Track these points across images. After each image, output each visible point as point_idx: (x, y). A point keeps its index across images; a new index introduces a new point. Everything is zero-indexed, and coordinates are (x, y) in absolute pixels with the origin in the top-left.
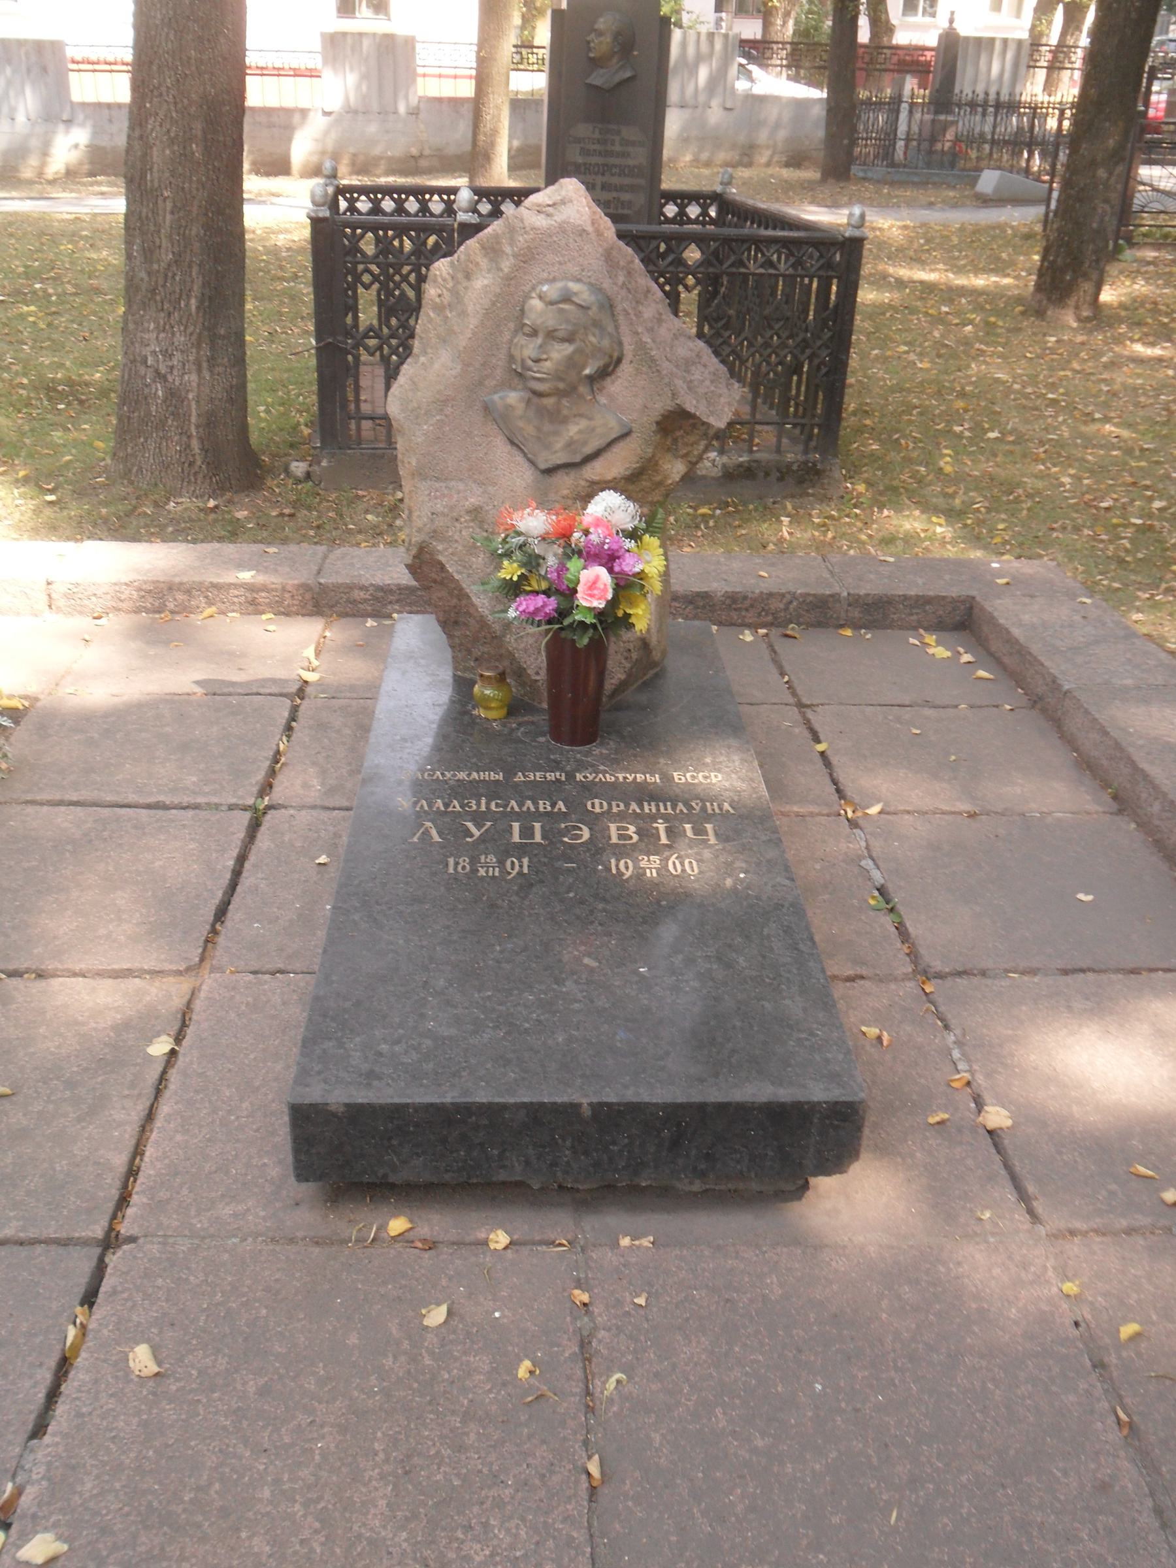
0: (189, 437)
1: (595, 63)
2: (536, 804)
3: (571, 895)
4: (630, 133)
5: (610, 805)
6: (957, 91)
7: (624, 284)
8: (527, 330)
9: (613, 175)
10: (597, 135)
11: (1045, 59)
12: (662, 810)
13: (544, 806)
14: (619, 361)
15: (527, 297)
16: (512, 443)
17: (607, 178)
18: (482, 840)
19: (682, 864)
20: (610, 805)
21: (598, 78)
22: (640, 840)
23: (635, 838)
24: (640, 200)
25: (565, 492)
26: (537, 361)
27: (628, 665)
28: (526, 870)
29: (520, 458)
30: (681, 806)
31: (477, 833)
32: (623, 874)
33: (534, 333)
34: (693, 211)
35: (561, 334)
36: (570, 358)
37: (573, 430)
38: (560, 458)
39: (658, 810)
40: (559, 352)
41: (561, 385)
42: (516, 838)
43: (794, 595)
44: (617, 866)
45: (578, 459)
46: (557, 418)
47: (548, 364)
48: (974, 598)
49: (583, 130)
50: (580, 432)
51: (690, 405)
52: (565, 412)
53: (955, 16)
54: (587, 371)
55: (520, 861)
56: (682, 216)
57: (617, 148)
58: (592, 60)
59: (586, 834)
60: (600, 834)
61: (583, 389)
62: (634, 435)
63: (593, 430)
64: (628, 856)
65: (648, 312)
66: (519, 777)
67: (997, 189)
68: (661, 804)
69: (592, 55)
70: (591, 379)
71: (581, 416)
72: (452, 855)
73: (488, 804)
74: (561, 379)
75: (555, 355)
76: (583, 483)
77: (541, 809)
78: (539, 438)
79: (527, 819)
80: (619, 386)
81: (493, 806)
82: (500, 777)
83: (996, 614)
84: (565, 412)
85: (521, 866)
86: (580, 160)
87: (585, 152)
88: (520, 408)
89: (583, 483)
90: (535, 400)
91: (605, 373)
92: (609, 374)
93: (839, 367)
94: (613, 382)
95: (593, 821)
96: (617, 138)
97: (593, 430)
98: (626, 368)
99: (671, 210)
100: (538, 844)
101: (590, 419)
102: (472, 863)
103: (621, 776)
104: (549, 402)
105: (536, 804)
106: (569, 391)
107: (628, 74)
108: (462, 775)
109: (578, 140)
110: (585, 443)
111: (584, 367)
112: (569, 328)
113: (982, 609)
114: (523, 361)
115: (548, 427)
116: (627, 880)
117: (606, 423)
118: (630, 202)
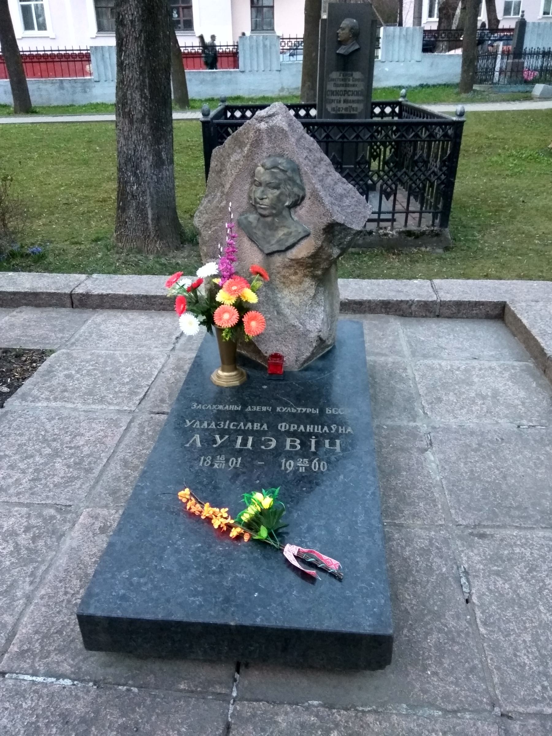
0: (148, 224)
1: (340, 43)
2: (253, 425)
3: (258, 482)
4: (357, 75)
5: (290, 426)
6: (524, 48)
7: (306, 157)
8: (257, 183)
9: (349, 95)
10: (341, 77)
11: (255, 48)
12: (316, 431)
13: (257, 426)
14: (303, 198)
15: (257, 166)
16: (252, 241)
17: (346, 97)
18: (221, 446)
19: (319, 465)
20: (290, 426)
21: (341, 50)
22: (301, 449)
23: (299, 447)
24: (360, 107)
25: (278, 264)
26: (262, 199)
27: (311, 349)
28: (238, 466)
29: (255, 248)
30: (326, 428)
31: (219, 441)
32: (287, 470)
33: (260, 184)
34: (388, 110)
35: (273, 185)
36: (278, 197)
37: (280, 233)
38: (275, 248)
39: (314, 430)
40: (272, 194)
41: (274, 212)
42: (238, 446)
43: (413, 301)
44: (285, 464)
45: (283, 248)
46: (273, 228)
47: (267, 200)
48: (505, 302)
49: (335, 75)
50: (284, 234)
51: (340, 218)
52: (277, 225)
53: (525, 13)
54: (287, 204)
55: (237, 460)
56: (382, 114)
57: (351, 82)
58: (340, 41)
59: (273, 444)
60: (281, 445)
61: (285, 213)
62: (312, 236)
63: (291, 233)
64: (293, 459)
65: (321, 170)
66: (249, 409)
67: (542, 93)
68: (316, 427)
69: (339, 39)
70: (289, 207)
71: (285, 226)
72: (203, 455)
73: (229, 424)
74: (274, 208)
75: (270, 196)
76: (287, 260)
77: (255, 429)
78: (264, 238)
79: (245, 434)
80: (302, 211)
81: (231, 427)
82: (239, 409)
83: (516, 312)
84: (277, 225)
85: (236, 463)
86: (334, 89)
87: (336, 85)
88: (255, 223)
89: (287, 260)
90: (262, 219)
91: (296, 204)
92: (299, 205)
93: (450, 185)
94: (301, 209)
95: (280, 436)
96: (351, 78)
97: (291, 233)
98: (307, 203)
99: (377, 110)
100: (248, 449)
101: (289, 228)
102: (212, 461)
103: (299, 409)
104: (269, 219)
105: (253, 425)
106: (278, 214)
107: (357, 47)
108: (221, 407)
109: (333, 80)
110: (287, 241)
111: (285, 202)
112: (277, 181)
113: (510, 309)
114: (255, 199)
115: (268, 232)
116: (288, 474)
117: (297, 230)
118: (357, 108)
